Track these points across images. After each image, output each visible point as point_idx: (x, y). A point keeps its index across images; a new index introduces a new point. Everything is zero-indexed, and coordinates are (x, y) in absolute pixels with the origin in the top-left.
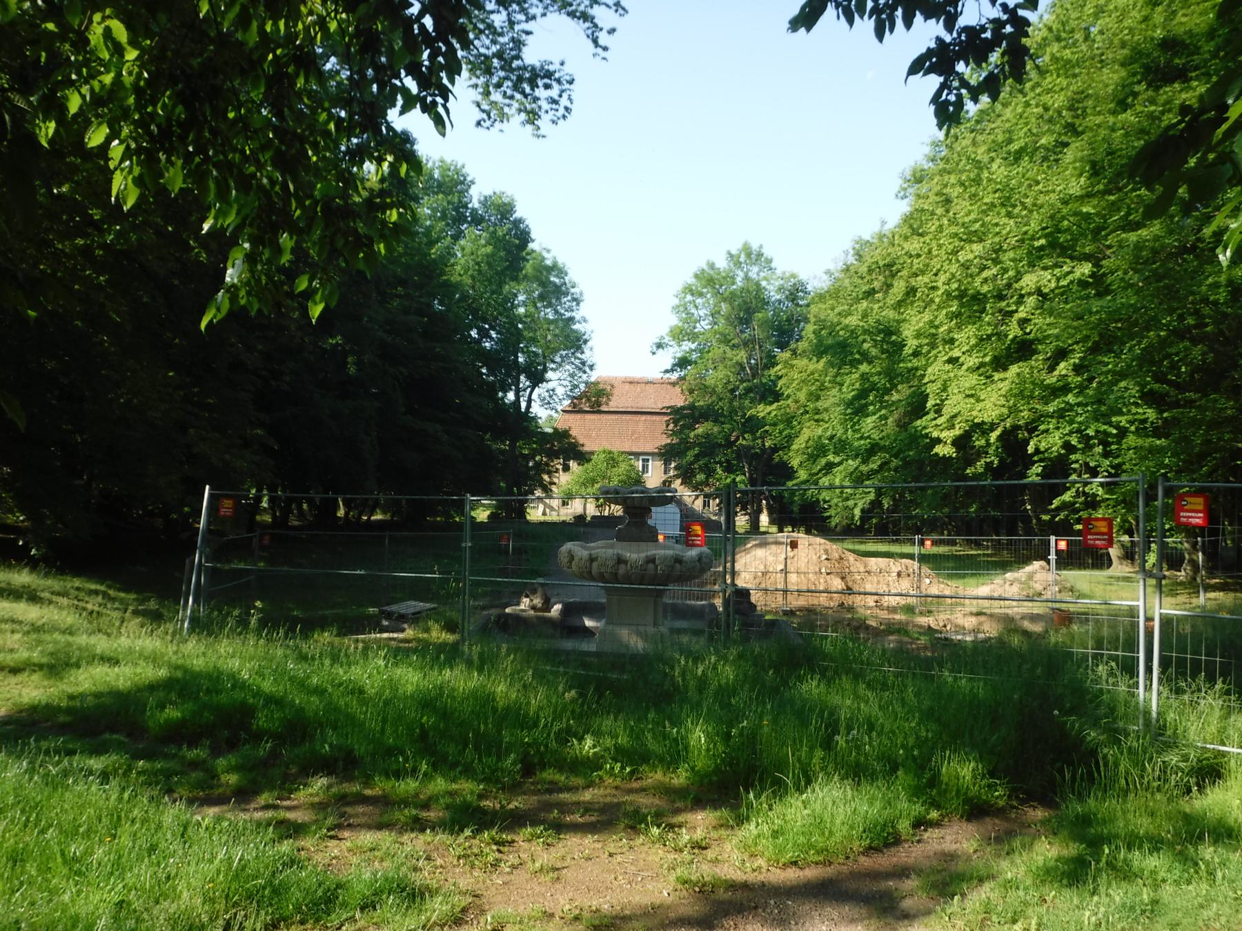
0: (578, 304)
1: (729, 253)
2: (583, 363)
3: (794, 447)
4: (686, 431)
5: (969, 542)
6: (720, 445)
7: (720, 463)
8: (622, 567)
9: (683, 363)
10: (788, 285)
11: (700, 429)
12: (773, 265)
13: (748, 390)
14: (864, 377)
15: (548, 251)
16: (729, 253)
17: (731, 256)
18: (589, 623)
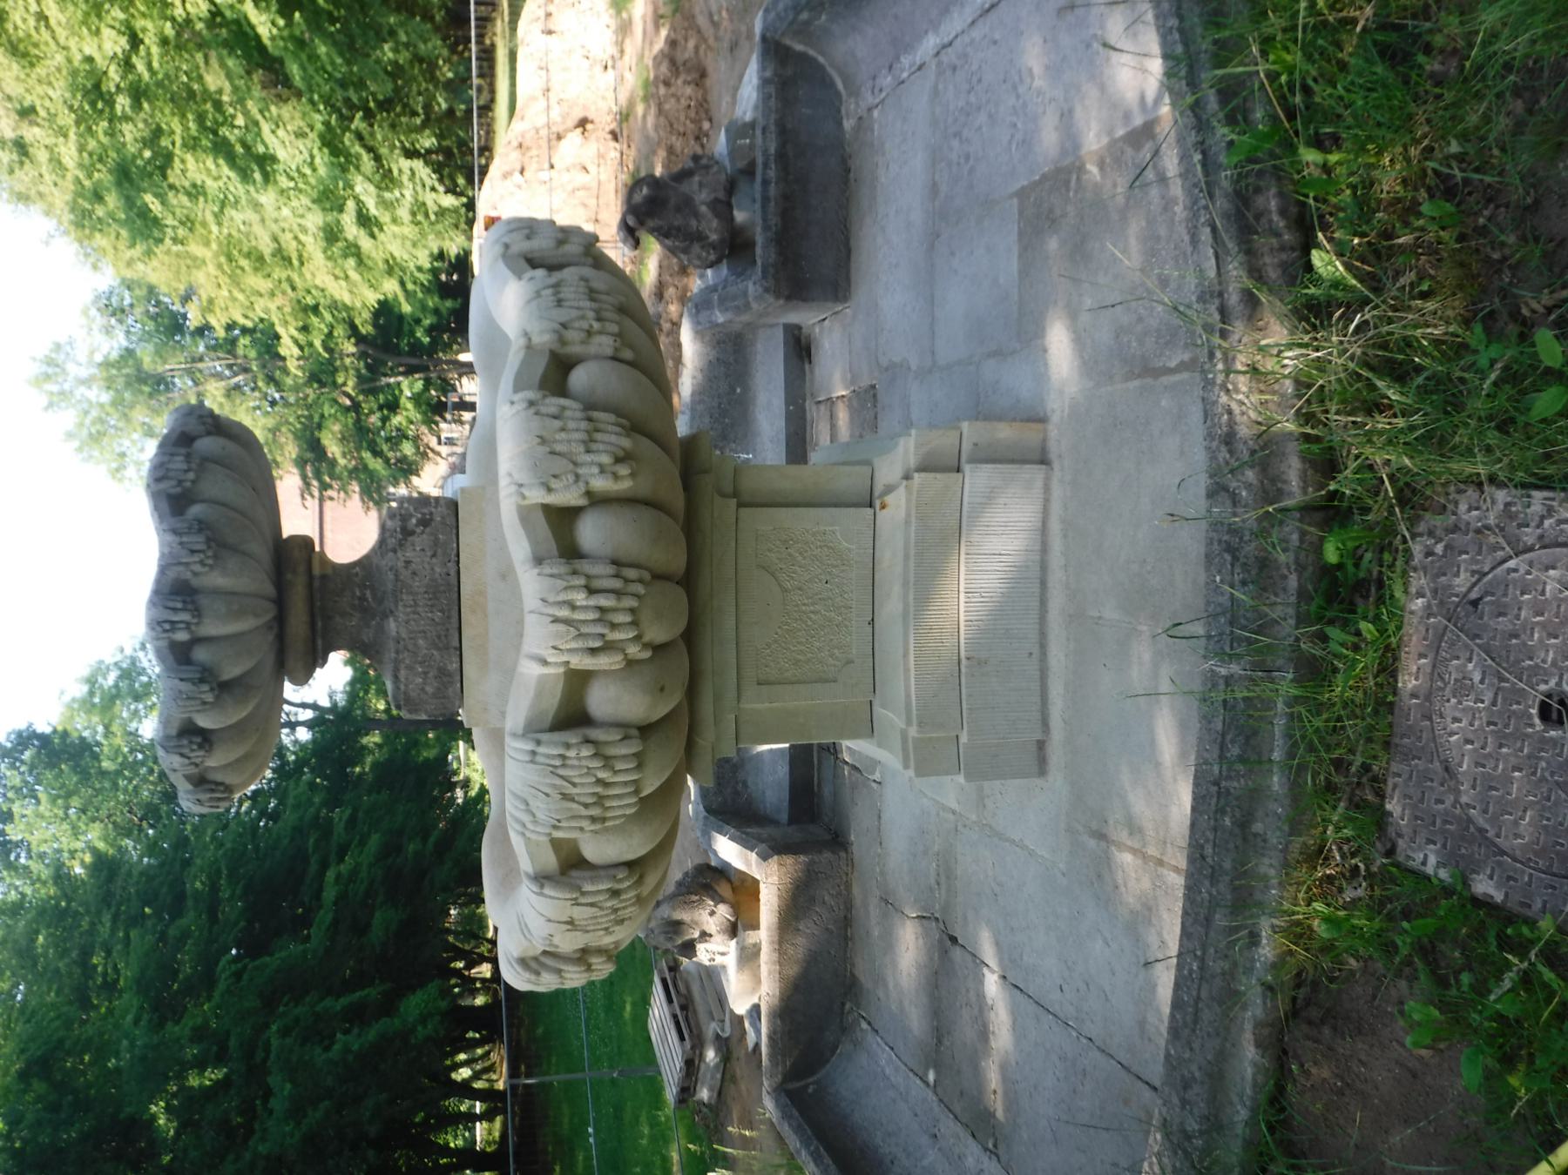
3: (347, 299)
4: (338, 470)
6: (358, 421)
7: (385, 420)
8: (603, 700)
10: (100, 320)
11: (333, 449)
12: (63, 340)
13: (271, 379)
14: (192, 145)
16: (46, 409)
17: (51, 405)
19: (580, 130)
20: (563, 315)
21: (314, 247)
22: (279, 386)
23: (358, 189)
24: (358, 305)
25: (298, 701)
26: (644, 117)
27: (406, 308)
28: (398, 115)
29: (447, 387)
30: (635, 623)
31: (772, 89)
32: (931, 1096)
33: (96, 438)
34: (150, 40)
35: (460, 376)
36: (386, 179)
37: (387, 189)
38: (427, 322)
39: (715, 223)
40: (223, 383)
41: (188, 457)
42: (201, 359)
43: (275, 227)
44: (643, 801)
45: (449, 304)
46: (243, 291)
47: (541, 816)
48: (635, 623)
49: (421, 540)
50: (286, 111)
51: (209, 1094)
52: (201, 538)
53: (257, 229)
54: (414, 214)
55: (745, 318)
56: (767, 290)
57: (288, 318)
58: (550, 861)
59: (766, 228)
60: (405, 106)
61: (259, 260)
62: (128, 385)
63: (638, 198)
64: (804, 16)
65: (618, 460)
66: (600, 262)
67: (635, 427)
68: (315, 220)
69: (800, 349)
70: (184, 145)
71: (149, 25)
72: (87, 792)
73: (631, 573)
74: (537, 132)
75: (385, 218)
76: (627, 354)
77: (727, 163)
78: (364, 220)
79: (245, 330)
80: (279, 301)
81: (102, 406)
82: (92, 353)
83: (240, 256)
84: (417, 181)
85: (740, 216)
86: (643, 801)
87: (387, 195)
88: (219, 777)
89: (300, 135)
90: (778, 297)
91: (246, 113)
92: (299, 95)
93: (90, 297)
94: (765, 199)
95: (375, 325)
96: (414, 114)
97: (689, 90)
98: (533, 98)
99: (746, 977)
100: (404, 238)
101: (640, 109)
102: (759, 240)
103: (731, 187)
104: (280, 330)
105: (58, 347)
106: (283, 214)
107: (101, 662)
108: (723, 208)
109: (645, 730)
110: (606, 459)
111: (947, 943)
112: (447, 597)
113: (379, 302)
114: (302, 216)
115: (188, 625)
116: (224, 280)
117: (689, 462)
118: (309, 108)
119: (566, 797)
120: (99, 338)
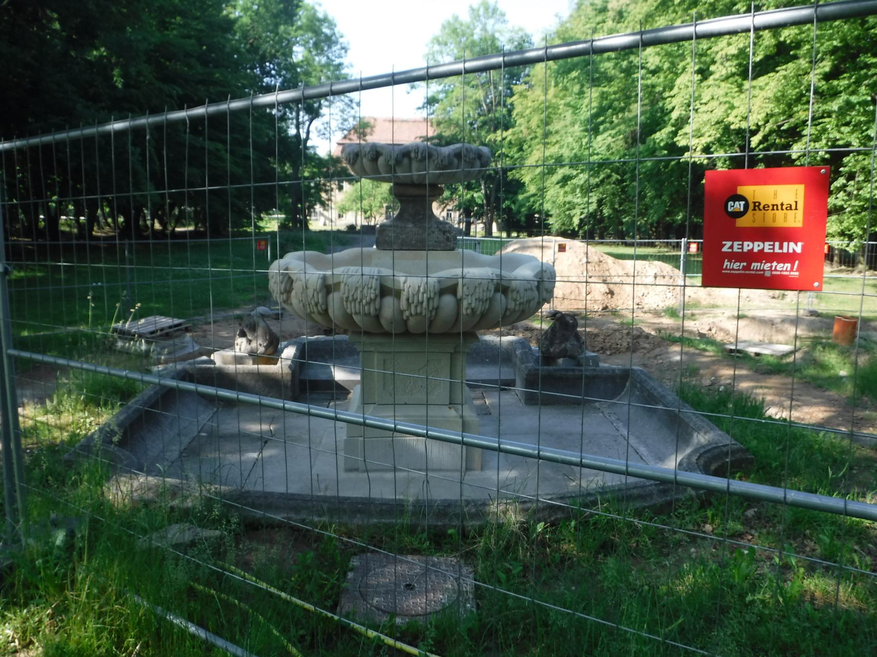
0: (346, 52)
1: (471, 7)
2: (351, 101)
5: (667, 244)
8: (389, 301)
9: (431, 101)
10: (517, 37)
12: (506, 18)
13: (484, 123)
14: (603, 96)
15: (320, 5)
16: (471, 7)
17: (473, 10)
18: (340, 375)
19: (608, 291)
20: (522, 291)
21: (553, 150)
22: (481, 128)
23: (581, 176)
24: (522, 172)
25: (311, 129)
26: (614, 323)
27: (521, 197)
28: (620, 196)
29: (479, 216)
30: (417, 314)
31: (611, 373)
32: (195, 434)
33: (454, 31)
34: (653, 80)
35: (484, 223)
36: (587, 190)
37: (582, 190)
38: (513, 207)
39: (557, 350)
40: (482, 98)
41: (474, 159)
42: (495, 88)
43: (563, 132)
44: (350, 316)
45: (523, 219)
46: (530, 113)
47: (350, 280)
48: (417, 314)
49: (442, 237)
50: (621, 143)
51: (109, 79)
52: (446, 163)
53: (562, 123)
54: (569, 203)
55: (518, 363)
56: (530, 370)
57: (516, 136)
58: (330, 282)
59: (555, 370)
60: (625, 200)
61: (547, 122)
62: (483, 50)
63: (568, 319)
64: (638, 385)
65: (472, 309)
66: (540, 305)
67: (483, 315)
68: (566, 153)
69: (505, 385)
70: (603, 93)
71: (661, 79)
72: (267, 15)
73: (434, 313)
74: (608, 270)
75: (567, 188)
76: (508, 313)
77: (583, 356)
78: (565, 180)
79: (510, 112)
80: (525, 131)
81: (472, 35)
82: (500, 32)
83: (548, 114)
84: (582, 206)
85: (560, 361)
86: (350, 316)
87: (578, 190)
88: (359, 161)
89: (609, 148)
90: (527, 375)
91: (618, 124)
92: (627, 149)
93: (529, 32)
94: (567, 370)
95: (512, 180)
96: (620, 205)
97: (625, 344)
98: (623, 269)
99: (230, 359)
100: (558, 197)
101: (618, 321)
102: (551, 368)
103: (572, 357)
104: (510, 131)
105: (503, 15)
106: (569, 138)
107: (335, 26)
108: (564, 354)
109: (377, 317)
110: (473, 305)
111: (263, 440)
112: (420, 245)
113: (524, 183)
114: (568, 146)
115: (416, 157)
116: (536, 104)
117: (471, 335)
118: (622, 153)
119: (357, 288)
120: (507, 36)
